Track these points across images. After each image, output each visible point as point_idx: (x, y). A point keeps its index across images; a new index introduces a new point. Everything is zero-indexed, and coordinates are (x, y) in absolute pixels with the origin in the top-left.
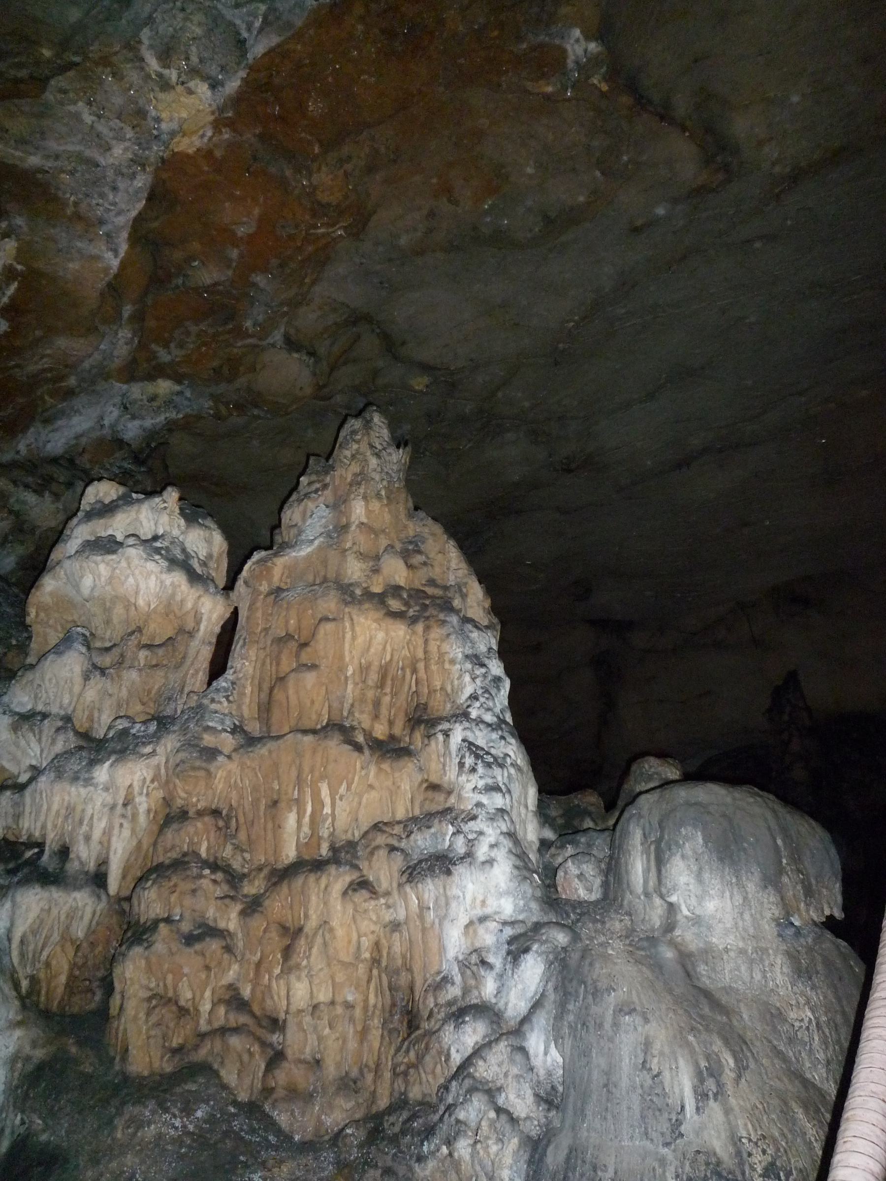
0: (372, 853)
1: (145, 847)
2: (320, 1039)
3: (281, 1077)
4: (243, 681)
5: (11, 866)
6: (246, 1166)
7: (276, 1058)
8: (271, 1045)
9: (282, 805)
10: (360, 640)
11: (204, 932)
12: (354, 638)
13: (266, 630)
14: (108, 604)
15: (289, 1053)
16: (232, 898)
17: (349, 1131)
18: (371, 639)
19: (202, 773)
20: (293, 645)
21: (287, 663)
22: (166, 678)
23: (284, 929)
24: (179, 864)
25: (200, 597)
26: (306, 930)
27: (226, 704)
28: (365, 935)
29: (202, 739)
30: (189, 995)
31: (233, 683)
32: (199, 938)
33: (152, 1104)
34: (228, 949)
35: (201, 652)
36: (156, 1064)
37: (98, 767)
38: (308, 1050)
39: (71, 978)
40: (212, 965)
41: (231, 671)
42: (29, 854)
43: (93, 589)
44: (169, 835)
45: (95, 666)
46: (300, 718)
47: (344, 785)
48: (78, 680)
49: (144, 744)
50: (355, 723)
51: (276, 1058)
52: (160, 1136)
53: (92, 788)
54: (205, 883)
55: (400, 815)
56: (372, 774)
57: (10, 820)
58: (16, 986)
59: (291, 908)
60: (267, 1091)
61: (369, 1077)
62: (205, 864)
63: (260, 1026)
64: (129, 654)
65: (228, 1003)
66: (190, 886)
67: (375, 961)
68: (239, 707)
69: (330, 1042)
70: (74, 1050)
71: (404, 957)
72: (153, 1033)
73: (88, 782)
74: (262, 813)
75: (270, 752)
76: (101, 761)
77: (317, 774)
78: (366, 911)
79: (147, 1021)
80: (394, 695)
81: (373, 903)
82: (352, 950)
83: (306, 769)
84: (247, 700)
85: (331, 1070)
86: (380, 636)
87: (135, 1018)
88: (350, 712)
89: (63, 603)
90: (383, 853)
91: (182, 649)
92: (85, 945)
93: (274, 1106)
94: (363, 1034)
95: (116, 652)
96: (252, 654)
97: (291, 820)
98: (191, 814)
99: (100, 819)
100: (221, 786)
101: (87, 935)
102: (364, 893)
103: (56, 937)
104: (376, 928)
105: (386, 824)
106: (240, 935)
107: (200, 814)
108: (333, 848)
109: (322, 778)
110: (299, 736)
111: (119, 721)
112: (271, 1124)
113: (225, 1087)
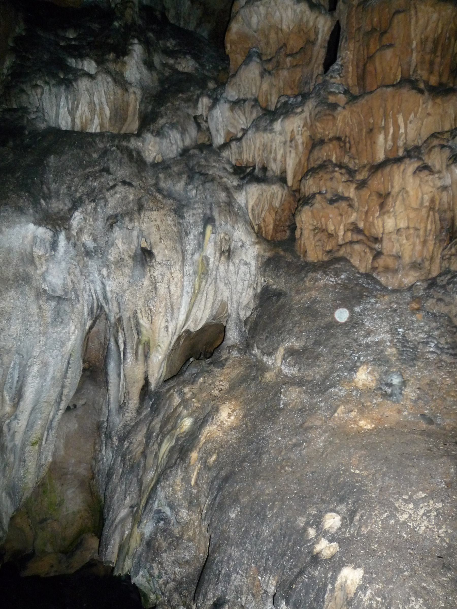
0: (430, 150)
1: (303, 161)
2: (401, 245)
3: (381, 262)
4: (347, 64)
5: (242, 176)
6: (367, 296)
7: (378, 254)
8: (375, 249)
9: (376, 130)
10: (421, 22)
11: (336, 199)
12: (417, 21)
13: (359, 29)
14: (267, 32)
15: (385, 252)
16: (351, 181)
17: (418, 284)
18: (428, 19)
19: (331, 117)
20: (377, 35)
21: (373, 47)
22: (302, 72)
23: (380, 195)
24: (323, 166)
25: (317, 17)
26: (392, 193)
27: (339, 78)
28: (427, 194)
29: (328, 99)
30: (333, 228)
31: (342, 66)
32: (336, 201)
33: (320, 272)
34: (351, 206)
35: (319, 53)
36: (320, 257)
37: (275, 123)
38: (394, 250)
39: (275, 226)
40: (343, 213)
41: (340, 59)
42: (248, 170)
43: (258, 24)
44: (316, 153)
45: (265, 70)
46: (383, 79)
47: (412, 115)
48: (258, 78)
49: (297, 107)
50: (418, 77)
51: (378, 254)
52: (326, 285)
53: (274, 134)
54: (337, 175)
55: (447, 127)
56: (429, 107)
57: (237, 156)
58: (253, 228)
59: (384, 183)
60: (374, 269)
61: (427, 263)
62: (336, 165)
63: (369, 240)
64: (281, 60)
65: (352, 230)
66: (329, 176)
67: (431, 208)
68: (346, 80)
69: (406, 247)
70: (282, 253)
71: (449, 204)
72: (317, 244)
73: (272, 131)
74: (363, 137)
75: (367, 101)
76: (276, 120)
77: (395, 110)
78: (427, 181)
79: (314, 239)
80: (443, 57)
81: (431, 177)
82: (419, 202)
83: (389, 108)
84: (350, 75)
85: (407, 259)
86: (435, 16)
87: (309, 238)
88: (415, 71)
89: (244, 37)
90: (437, 150)
91: (309, 53)
92: (280, 211)
93: (378, 274)
94: (425, 243)
95: (275, 60)
96: (351, 46)
97: (381, 138)
98: (326, 140)
99: (279, 150)
100: (340, 124)
101: (280, 206)
102: (426, 172)
103: (267, 207)
104: (433, 190)
105: (439, 133)
106: (356, 200)
107: (331, 140)
108: (406, 150)
109: (398, 112)
110: (384, 89)
111: (282, 98)
112: (377, 282)
113: (353, 266)
